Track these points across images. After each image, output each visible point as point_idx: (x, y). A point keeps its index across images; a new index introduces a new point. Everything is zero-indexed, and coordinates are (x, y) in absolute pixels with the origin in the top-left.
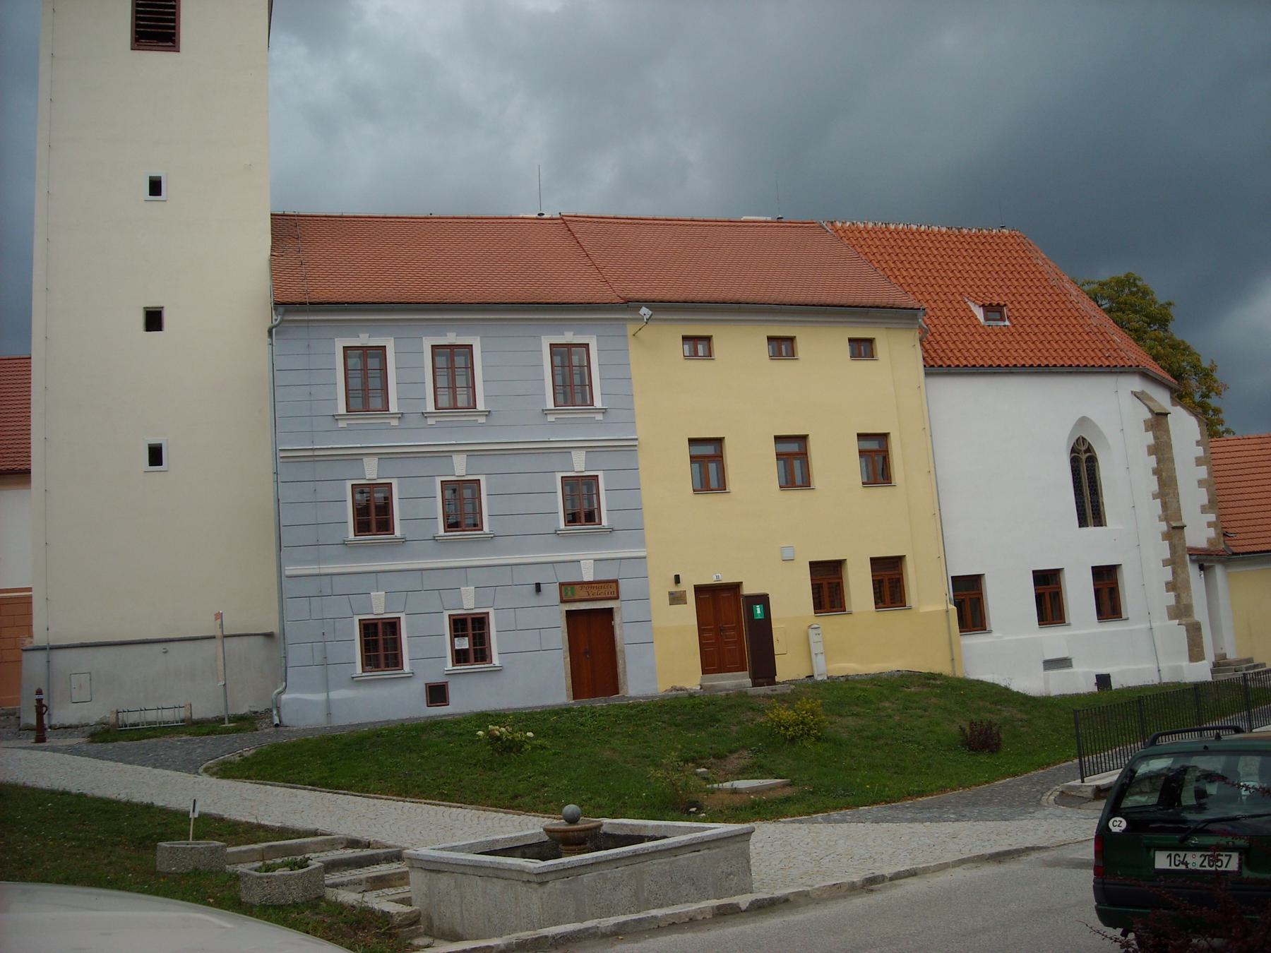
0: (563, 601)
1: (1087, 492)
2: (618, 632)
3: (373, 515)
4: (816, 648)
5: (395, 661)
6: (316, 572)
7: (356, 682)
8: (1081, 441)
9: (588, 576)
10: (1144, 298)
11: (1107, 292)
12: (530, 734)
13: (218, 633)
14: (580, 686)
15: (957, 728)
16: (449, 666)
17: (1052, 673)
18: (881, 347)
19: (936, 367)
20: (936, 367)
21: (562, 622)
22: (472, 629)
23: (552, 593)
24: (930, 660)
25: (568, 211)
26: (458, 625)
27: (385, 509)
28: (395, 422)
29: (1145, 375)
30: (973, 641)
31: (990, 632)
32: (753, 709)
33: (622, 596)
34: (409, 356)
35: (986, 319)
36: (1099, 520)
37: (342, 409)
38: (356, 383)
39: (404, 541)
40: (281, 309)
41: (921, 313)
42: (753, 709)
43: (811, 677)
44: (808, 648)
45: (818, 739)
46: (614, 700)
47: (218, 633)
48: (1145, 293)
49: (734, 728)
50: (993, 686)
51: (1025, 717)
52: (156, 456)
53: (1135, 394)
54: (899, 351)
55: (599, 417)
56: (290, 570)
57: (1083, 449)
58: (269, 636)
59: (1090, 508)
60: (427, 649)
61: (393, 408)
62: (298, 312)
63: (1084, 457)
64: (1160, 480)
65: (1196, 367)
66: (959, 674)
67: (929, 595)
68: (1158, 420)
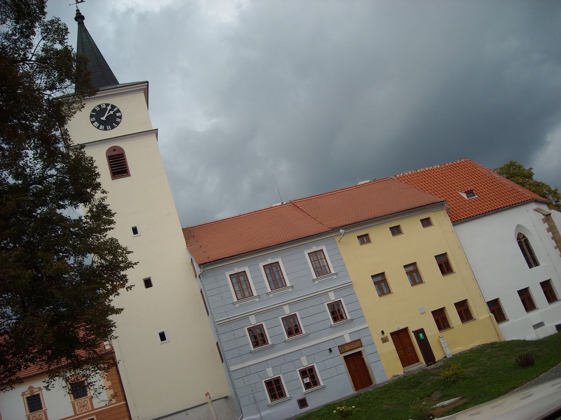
0: (341, 353)
1: (528, 254)
2: (366, 360)
3: (258, 338)
4: (444, 345)
5: (282, 394)
6: (243, 366)
7: (269, 406)
8: (520, 234)
9: (348, 340)
10: (520, 169)
11: (504, 171)
12: (353, 407)
13: (209, 401)
14: (357, 386)
15: (514, 360)
16: (304, 390)
17: (538, 330)
18: (433, 220)
19: (456, 222)
20: (456, 222)
21: (343, 361)
22: (308, 373)
23: (336, 351)
24: (491, 338)
25: (292, 199)
26: (304, 373)
27: (263, 335)
28: (257, 300)
29: (536, 201)
30: (503, 325)
31: (508, 320)
32: (432, 375)
33: (364, 345)
34: (255, 272)
35: (468, 197)
36: (536, 264)
37: (235, 300)
38: (237, 288)
39: (273, 345)
40: (202, 266)
41: (445, 202)
42: (432, 375)
43: (445, 357)
44: (450, 344)
45: (464, 379)
46: (370, 389)
47: (209, 401)
48: (520, 167)
49: (428, 384)
50: (519, 341)
51: (537, 349)
52: (162, 337)
53: (535, 210)
54: (440, 219)
55: (335, 277)
56: (232, 368)
57: (521, 237)
58: (226, 397)
59: (532, 260)
60: (294, 387)
61: (255, 294)
62: (209, 266)
63: (523, 240)
64: (556, 241)
65: (550, 191)
66: (502, 340)
67: (481, 313)
68: (547, 218)
